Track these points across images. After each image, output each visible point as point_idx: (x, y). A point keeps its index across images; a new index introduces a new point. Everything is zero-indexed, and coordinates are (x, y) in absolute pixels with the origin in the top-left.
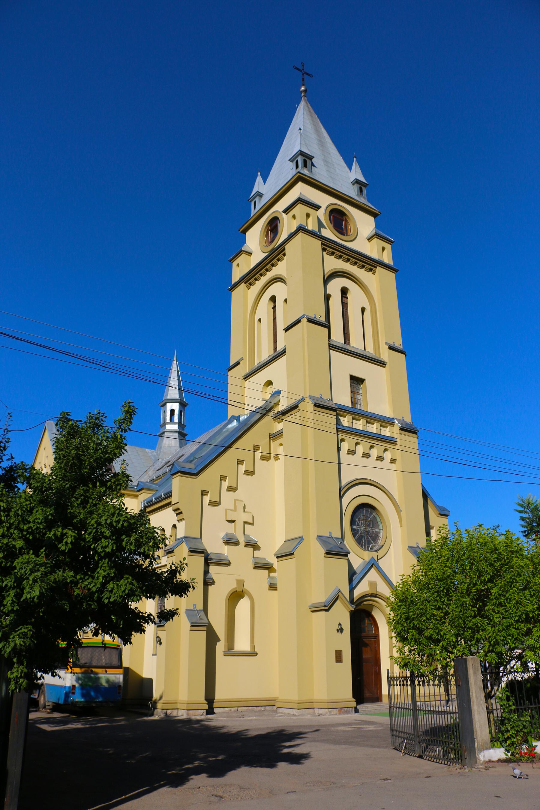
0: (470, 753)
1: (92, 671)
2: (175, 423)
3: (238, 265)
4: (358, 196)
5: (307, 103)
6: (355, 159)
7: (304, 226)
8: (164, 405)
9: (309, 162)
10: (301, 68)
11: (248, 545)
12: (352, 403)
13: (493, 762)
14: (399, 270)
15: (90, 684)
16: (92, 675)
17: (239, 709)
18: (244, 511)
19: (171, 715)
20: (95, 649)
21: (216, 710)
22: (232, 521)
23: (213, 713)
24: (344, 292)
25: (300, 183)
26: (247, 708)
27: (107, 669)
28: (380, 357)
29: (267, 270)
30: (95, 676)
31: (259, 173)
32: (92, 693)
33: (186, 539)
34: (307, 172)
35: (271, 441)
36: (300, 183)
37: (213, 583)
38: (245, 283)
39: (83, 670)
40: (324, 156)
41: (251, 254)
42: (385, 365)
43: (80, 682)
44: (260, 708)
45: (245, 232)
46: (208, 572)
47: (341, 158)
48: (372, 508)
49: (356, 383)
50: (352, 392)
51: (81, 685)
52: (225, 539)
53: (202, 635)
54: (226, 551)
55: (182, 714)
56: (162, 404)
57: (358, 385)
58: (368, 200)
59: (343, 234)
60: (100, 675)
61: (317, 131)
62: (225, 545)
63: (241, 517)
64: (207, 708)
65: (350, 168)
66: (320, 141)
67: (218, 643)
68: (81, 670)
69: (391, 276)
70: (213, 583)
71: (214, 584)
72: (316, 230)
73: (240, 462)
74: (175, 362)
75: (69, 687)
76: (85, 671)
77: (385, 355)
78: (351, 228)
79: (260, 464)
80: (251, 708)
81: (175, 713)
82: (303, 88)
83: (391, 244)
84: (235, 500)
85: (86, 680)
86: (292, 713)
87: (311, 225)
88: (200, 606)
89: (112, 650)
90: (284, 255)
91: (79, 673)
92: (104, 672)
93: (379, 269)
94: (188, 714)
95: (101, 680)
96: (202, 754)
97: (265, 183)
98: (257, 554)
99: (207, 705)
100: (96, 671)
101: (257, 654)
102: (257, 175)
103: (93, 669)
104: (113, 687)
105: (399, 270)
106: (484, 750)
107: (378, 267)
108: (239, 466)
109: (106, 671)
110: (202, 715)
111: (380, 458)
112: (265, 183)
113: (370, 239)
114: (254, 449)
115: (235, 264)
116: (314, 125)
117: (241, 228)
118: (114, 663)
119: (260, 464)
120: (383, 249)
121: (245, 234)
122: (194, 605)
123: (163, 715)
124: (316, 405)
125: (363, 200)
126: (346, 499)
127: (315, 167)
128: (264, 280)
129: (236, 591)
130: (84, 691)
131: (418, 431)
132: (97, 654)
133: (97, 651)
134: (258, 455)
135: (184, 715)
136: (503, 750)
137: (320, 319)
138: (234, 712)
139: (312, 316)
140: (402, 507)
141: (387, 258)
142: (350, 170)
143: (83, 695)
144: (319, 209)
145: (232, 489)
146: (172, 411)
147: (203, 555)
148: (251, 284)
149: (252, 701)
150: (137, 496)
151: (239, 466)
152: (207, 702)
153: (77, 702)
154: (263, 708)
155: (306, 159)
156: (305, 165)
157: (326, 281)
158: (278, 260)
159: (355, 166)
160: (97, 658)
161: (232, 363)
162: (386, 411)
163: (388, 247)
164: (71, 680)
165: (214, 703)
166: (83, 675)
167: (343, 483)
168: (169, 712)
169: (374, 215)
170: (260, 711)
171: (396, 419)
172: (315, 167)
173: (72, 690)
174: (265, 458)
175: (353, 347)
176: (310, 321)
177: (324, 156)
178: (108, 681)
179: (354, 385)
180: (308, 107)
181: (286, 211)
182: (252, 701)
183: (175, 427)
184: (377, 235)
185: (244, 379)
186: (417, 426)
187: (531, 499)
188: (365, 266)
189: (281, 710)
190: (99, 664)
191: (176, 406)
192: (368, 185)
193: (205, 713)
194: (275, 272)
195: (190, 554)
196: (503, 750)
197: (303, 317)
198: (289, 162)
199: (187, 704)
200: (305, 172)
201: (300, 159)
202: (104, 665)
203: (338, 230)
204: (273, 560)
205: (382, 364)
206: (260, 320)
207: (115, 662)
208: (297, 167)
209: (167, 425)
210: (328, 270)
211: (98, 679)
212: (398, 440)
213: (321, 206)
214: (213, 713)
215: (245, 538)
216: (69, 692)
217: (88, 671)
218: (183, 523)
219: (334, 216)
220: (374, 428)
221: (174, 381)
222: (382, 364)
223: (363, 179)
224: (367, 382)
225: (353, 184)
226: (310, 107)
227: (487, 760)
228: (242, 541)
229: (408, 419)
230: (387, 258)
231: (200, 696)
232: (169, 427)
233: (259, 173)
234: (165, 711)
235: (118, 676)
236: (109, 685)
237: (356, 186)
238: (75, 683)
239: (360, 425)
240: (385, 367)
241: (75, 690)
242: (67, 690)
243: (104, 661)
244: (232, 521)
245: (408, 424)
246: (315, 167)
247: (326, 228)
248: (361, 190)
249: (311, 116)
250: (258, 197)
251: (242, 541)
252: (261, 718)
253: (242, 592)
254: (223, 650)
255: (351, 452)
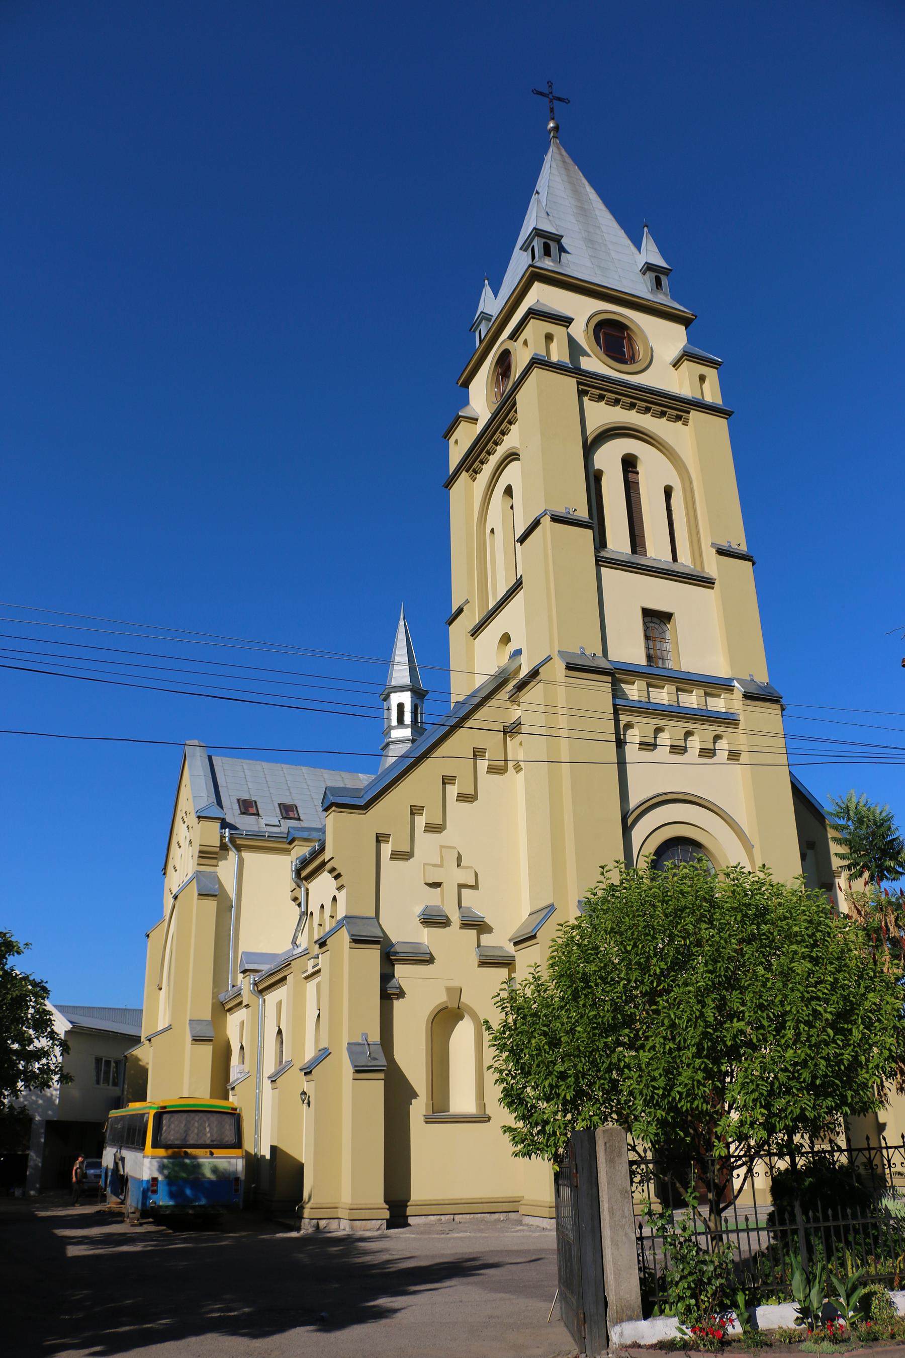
0: (591, 1328)
1: (186, 1153)
2: (407, 727)
3: (456, 442)
4: (652, 292)
5: (558, 148)
6: (646, 229)
7: (541, 356)
8: (387, 698)
9: (554, 247)
10: (546, 91)
11: (465, 925)
12: (649, 658)
13: (639, 1346)
14: (733, 412)
15: (184, 1175)
16: (187, 1161)
17: (457, 1217)
18: (459, 866)
19: (327, 1229)
20: (192, 1115)
21: (411, 1220)
22: (437, 885)
23: (406, 1224)
24: (629, 463)
25: (536, 283)
26: (472, 1216)
27: (213, 1150)
28: (703, 570)
29: (496, 444)
30: (192, 1163)
31: (486, 282)
32: (188, 1192)
33: (348, 920)
34: (551, 264)
35: (508, 739)
36: (536, 283)
37: (401, 994)
38: (467, 471)
39: (170, 1151)
40: (589, 232)
41: (477, 420)
42: (713, 583)
43: (166, 1172)
44: (496, 1216)
45: (466, 384)
46: (392, 976)
47: (622, 233)
48: (697, 845)
49: (658, 621)
50: (647, 638)
51: (167, 1177)
52: (422, 917)
53: (376, 1088)
54: (425, 937)
55: (342, 1228)
56: (382, 697)
57: (663, 627)
58: (673, 297)
59: (623, 361)
60: (201, 1160)
61: (576, 192)
62: (424, 927)
63: (453, 876)
64: (388, 1217)
65: (638, 246)
66: (582, 208)
67: (413, 1101)
68: (166, 1151)
69: (720, 425)
70: (401, 994)
71: (403, 997)
72: (566, 359)
73: (447, 780)
74: (401, 623)
75: (148, 1181)
76: (174, 1153)
77: (712, 565)
78: (640, 348)
79: (486, 780)
80: (479, 1215)
81: (334, 1225)
82: (552, 125)
83: (717, 368)
84: (442, 847)
85: (176, 1169)
86: (542, 1226)
87: (558, 353)
88: (375, 1036)
89: (224, 1116)
90: (516, 412)
91: (165, 1157)
92: (208, 1155)
93: (694, 415)
94: (352, 1228)
95: (203, 1168)
96: (247, 1307)
97: (496, 297)
98: (486, 939)
99: (388, 1212)
100: (194, 1153)
101: (489, 1118)
102: (484, 285)
103: (189, 1151)
104: (226, 1180)
105: (733, 412)
106: (622, 1321)
107: (692, 411)
108: (448, 786)
109: (212, 1154)
110: (379, 1229)
111: (708, 753)
112: (496, 297)
113: (676, 364)
114: (475, 755)
115: (452, 441)
116: (570, 183)
117: (459, 379)
118: (227, 1139)
119: (486, 780)
120: (702, 378)
121: (468, 388)
122: (363, 1034)
123: (311, 1230)
124: (570, 667)
125: (662, 299)
126: (638, 834)
127: (568, 253)
128: (494, 460)
129: (447, 1008)
130: (174, 1189)
131: (781, 698)
132: (196, 1124)
133: (197, 1118)
134: (483, 765)
135: (347, 1229)
136: (675, 1321)
137: (575, 513)
138: (447, 1222)
139: (561, 510)
140: (755, 839)
141: (711, 394)
142: (639, 248)
143: (172, 1195)
144: (570, 323)
145: (433, 828)
146: (401, 707)
147: (379, 946)
148: (476, 473)
149: (482, 1203)
150: (287, 851)
151: (448, 786)
152: (387, 1207)
153: (161, 1207)
154: (502, 1217)
155: (548, 241)
156: (547, 252)
157: (589, 448)
158: (510, 423)
159: (648, 243)
160: (196, 1131)
161: (454, 609)
162: (720, 668)
163: (712, 374)
164: (150, 1169)
165: (408, 1209)
166: (170, 1160)
167: (633, 803)
168: (322, 1223)
169: (686, 322)
170: (499, 1220)
171: (739, 680)
172: (568, 253)
173: (153, 1185)
174: (495, 770)
175: (650, 558)
176: (556, 519)
177: (589, 232)
178: (215, 1170)
179: (653, 625)
180: (561, 154)
181: (513, 336)
182: (482, 1203)
183: (407, 733)
184: (687, 355)
185: (472, 635)
186: (780, 690)
187: (854, 800)
188: (650, 408)
189: (527, 1220)
190: (200, 1142)
191: (406, 698)
192: (671, 270)
193: (385, 1226)
194: (510, 441)
195: (354, 945)
196: (675, 1321)
197: (544, 514)
198: (522, 252)
199: (350, 1209)
200: (548, 264)
201: (537, 244)
202: (208, 1142)
203: (615, 355)
204: (510, 949)
205: (706, 582)
206: (492, 531)
207: (230, 1137)
208: (533, 257)
209: (392, 732)
210: (592, 428)
211: (198, 1166)
212: (741, 718)
213: (573, 316)
214: (406, 1224)
215: (460, 913)
216: (148, 1189)
217: (179, 1152)
218: (344, 891)
219: (605, 334)
220: (692, 700)
221: (401, 654)
222: (706, 582)
223: (661, 263)
224: (677, 618)
225: (644, 274)
226: (564, 153)
227: (629, 1342)
228: (455, 917)
229: (762, 677)
230: (711, 394)
231: (376, 1195)
232: (397, 734)
233: (486, 282)
234: (315, 1222)
235: (233, 1161)
236: (217, 1177)
237: (650, 275)
238: (156, 1174)
239: (663, 696)
240: (713, 588)
241: (157, 1185)
242: (145, 1185)
243: (209, 1135)
244: (437, 885)
245: (761, 687)
246: (568, 253)
247: (589, 356)
248: (658, 283)
249: (567, 169)
250: (484, 321)
251: (455, 917)
252: (484, 1235)
253: (458, 1008)
254: (424, 1113)
255: (648, 746)
